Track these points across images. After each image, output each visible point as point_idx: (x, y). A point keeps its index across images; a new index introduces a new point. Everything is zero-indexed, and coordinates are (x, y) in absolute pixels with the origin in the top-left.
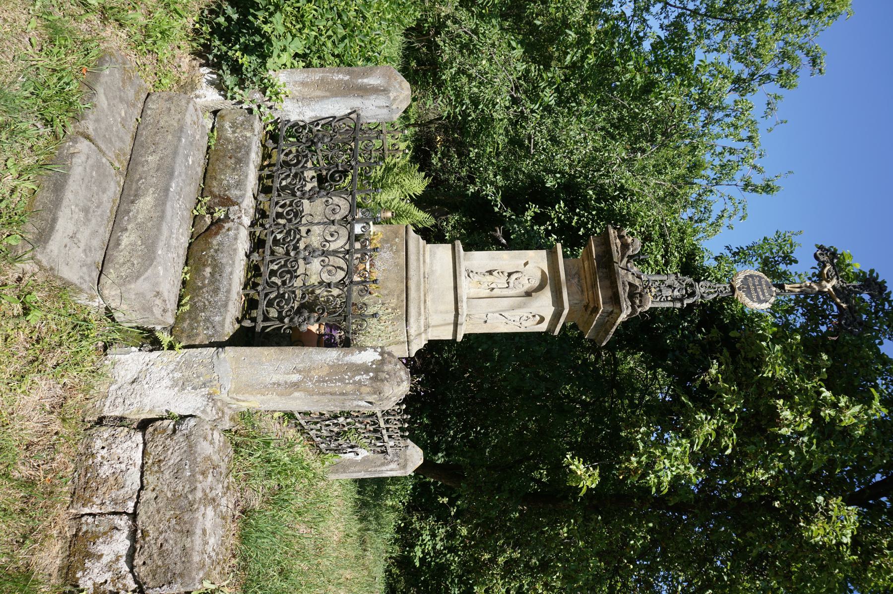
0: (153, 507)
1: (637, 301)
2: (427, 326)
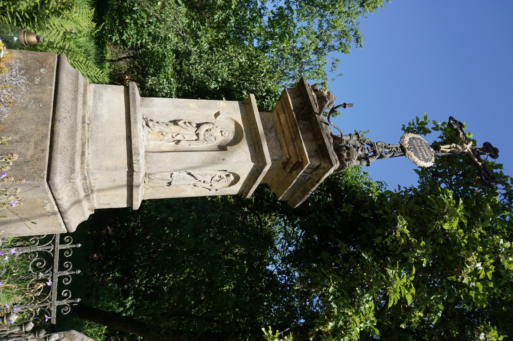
2: (89, 191)
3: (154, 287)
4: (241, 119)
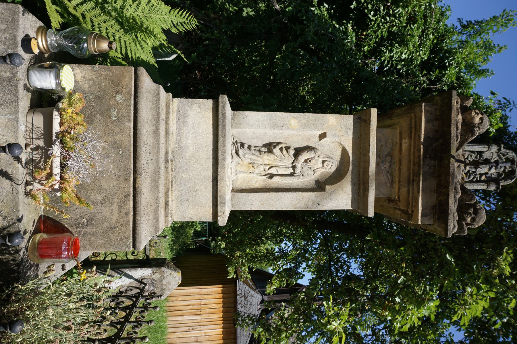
1: (469, 220)
4: (351, 145)
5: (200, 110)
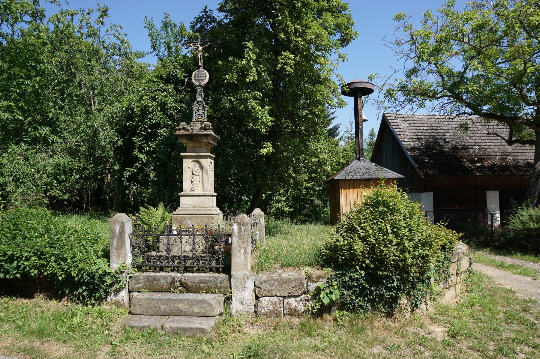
0: (282, 291)
3: (237, 182)
5: (183, 200)
